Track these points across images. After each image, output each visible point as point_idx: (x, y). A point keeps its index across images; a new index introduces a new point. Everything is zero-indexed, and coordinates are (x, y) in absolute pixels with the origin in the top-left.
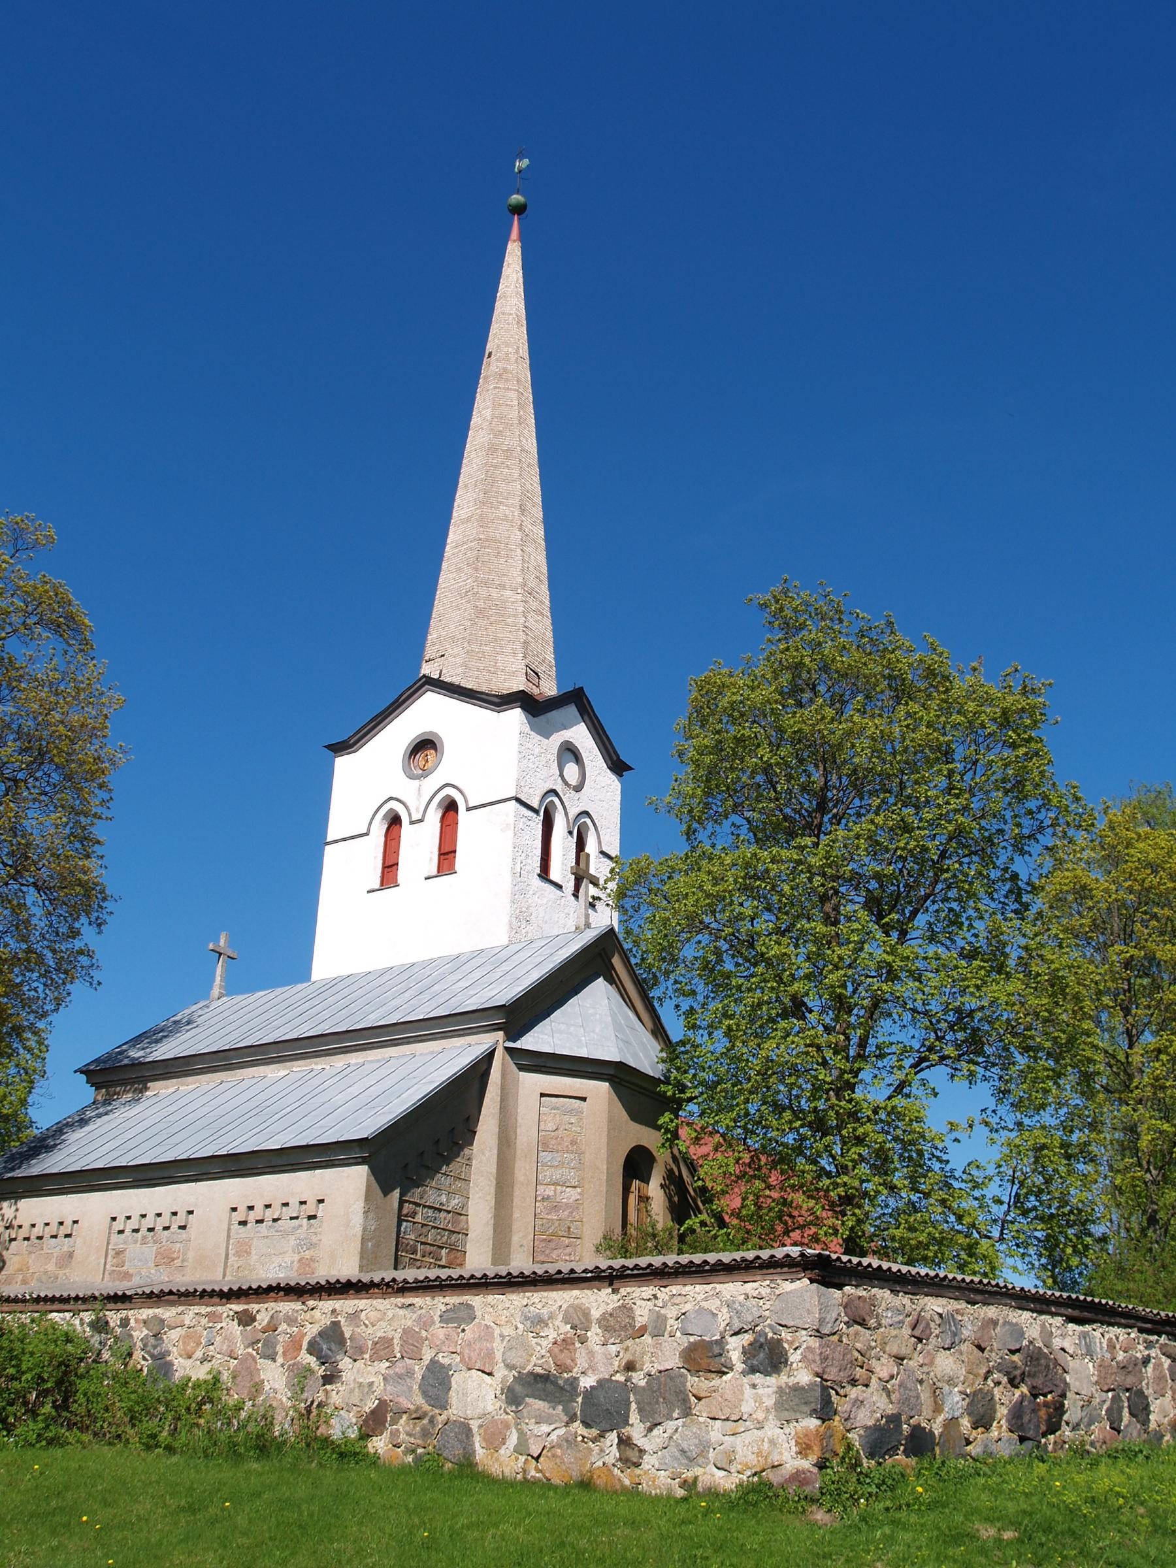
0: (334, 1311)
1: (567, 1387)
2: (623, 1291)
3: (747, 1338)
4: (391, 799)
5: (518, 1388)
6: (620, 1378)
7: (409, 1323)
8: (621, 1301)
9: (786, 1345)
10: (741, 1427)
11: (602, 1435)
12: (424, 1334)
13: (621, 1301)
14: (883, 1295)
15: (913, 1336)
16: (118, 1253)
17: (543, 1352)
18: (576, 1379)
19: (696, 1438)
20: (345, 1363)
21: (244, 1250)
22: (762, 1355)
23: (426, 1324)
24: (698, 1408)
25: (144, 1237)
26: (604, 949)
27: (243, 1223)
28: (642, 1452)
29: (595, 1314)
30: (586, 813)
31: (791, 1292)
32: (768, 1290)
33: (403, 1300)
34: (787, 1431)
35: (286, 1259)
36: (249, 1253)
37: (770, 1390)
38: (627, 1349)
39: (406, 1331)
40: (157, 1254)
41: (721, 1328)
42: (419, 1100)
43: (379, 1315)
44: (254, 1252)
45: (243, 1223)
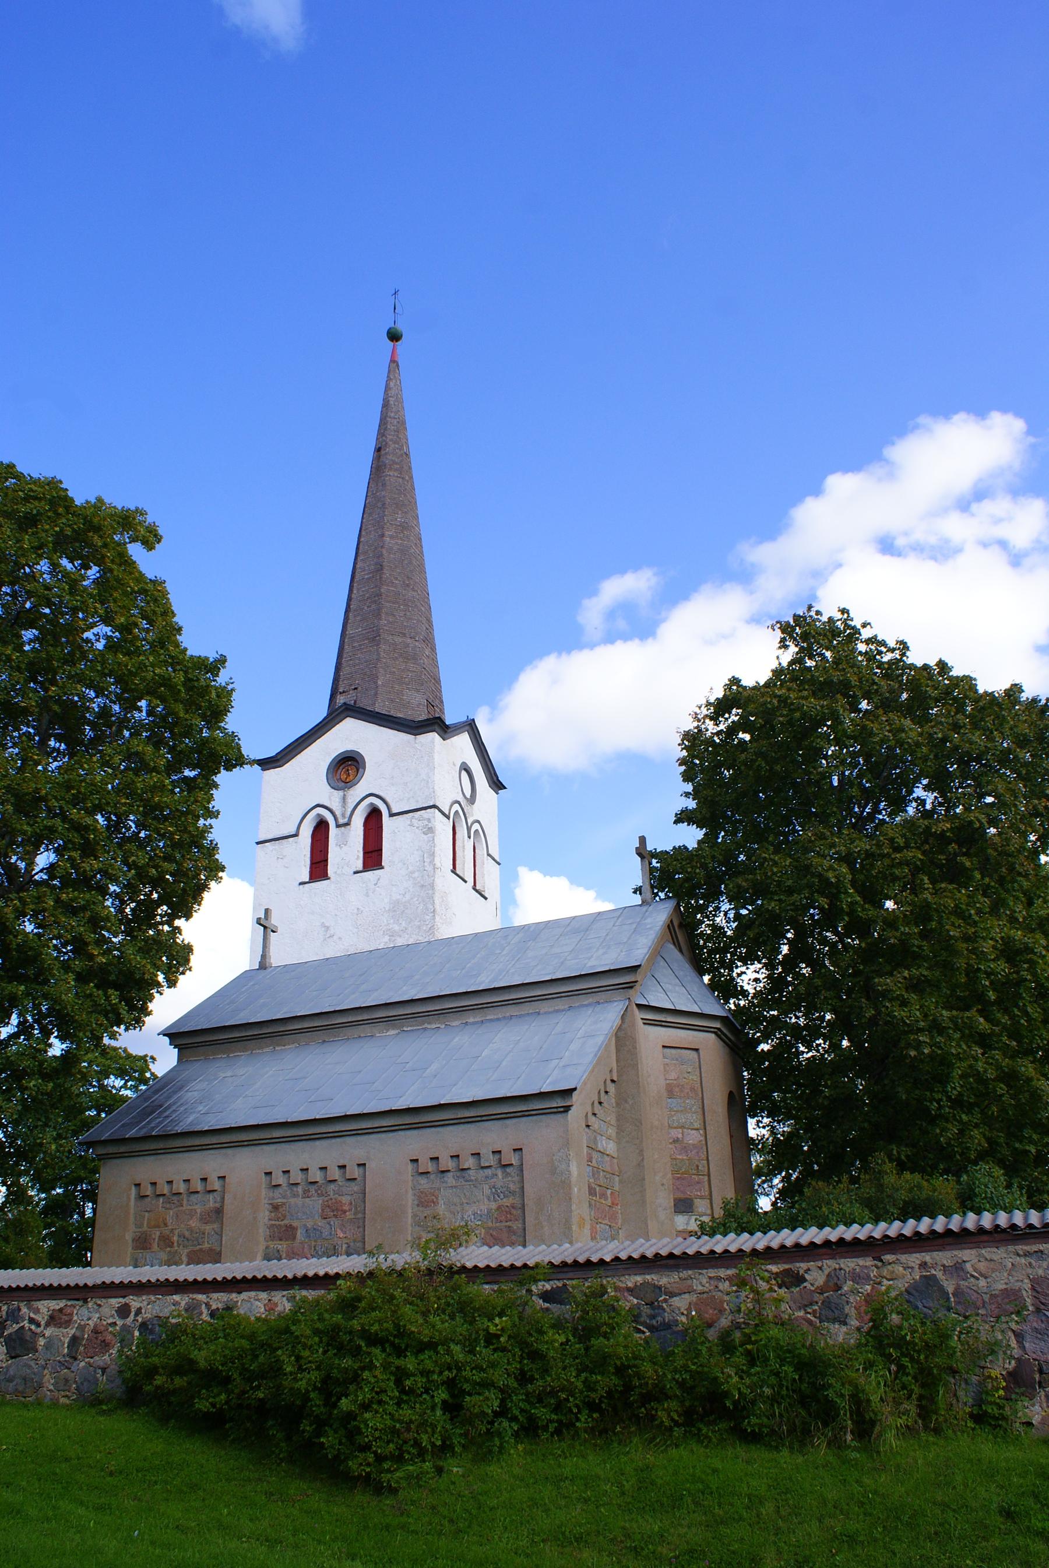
4: (318, 806)
25: (306, 1192)
30: (478, 822)
33: (1027, 1248)
35: (482, 1207)
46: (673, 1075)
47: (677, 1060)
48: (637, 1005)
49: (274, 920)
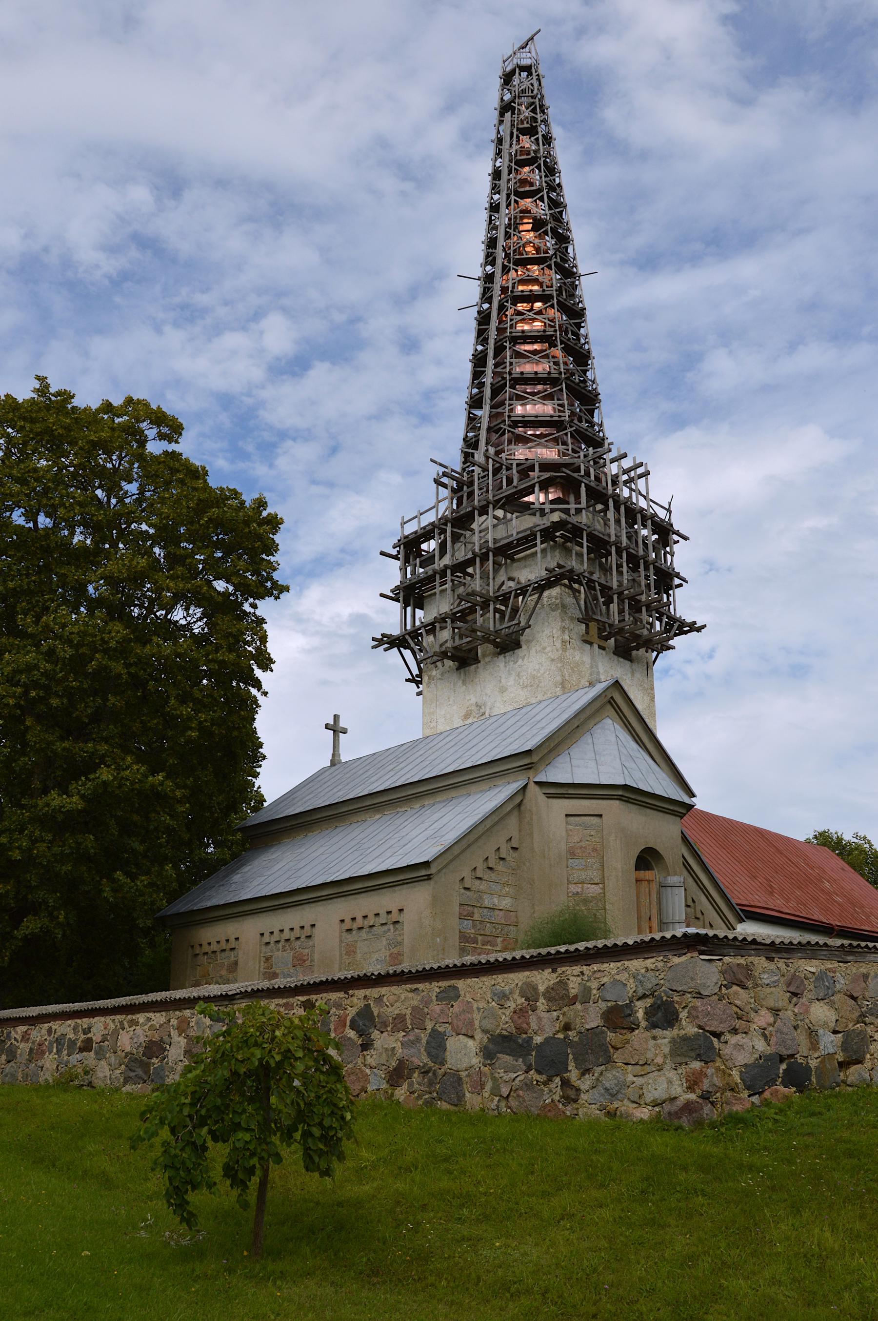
0: (365, 997)
1: (525, 1045)
2: (560, 970)
3: (649, 1002)
5: (491, 1046)
6: (561, 1036)
7: (415, 1003)
8: (559, 978)
9: (676, 1006)
10: (647, 1068)
11: (550, 1080)
12: (426, 1010)
13: (559, 978)
14: (760, 962)
15: (788, 992)
16: (268, 959)
17: (507, 1019)
18: (531, 1038)
19: (615, 1079)
20: (375, 1034)
21: (351, 951)
22: (660, 1014)
23: (427, 1003)
24: (617, 1056)
25: (284, 946)
26: (612, 698)
27: (349, 930)
28: (578, 1090)
29: (542, 988)
31: (679, 964)
32: (662, 964)
34: (680, 1071)
36: (355, 952)
37: (666, 1041)
38: (564, 1014)
39: (414, 1009)
40: (294, 957)
41: (630, 995)
42: (467, 829)
43: (395, 998)
44: (358, 951)
45: (349, 930)
46: (576, 839)
47: (580, 825)
48: (536, 783)
49: (342, 724)
